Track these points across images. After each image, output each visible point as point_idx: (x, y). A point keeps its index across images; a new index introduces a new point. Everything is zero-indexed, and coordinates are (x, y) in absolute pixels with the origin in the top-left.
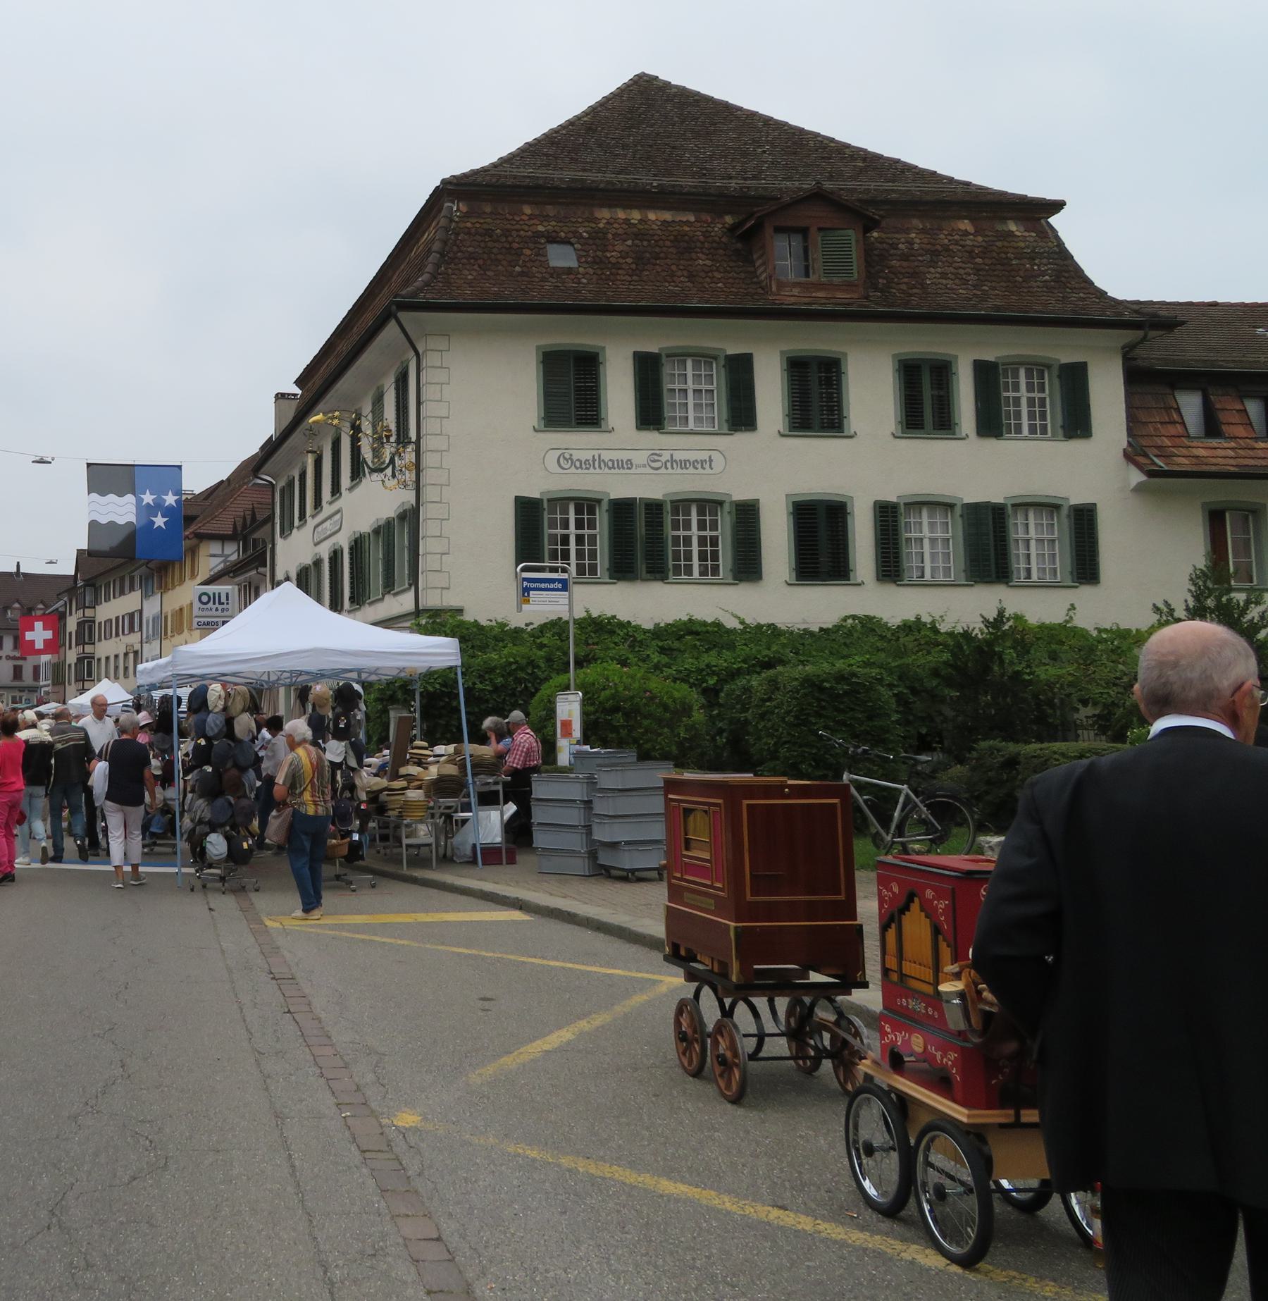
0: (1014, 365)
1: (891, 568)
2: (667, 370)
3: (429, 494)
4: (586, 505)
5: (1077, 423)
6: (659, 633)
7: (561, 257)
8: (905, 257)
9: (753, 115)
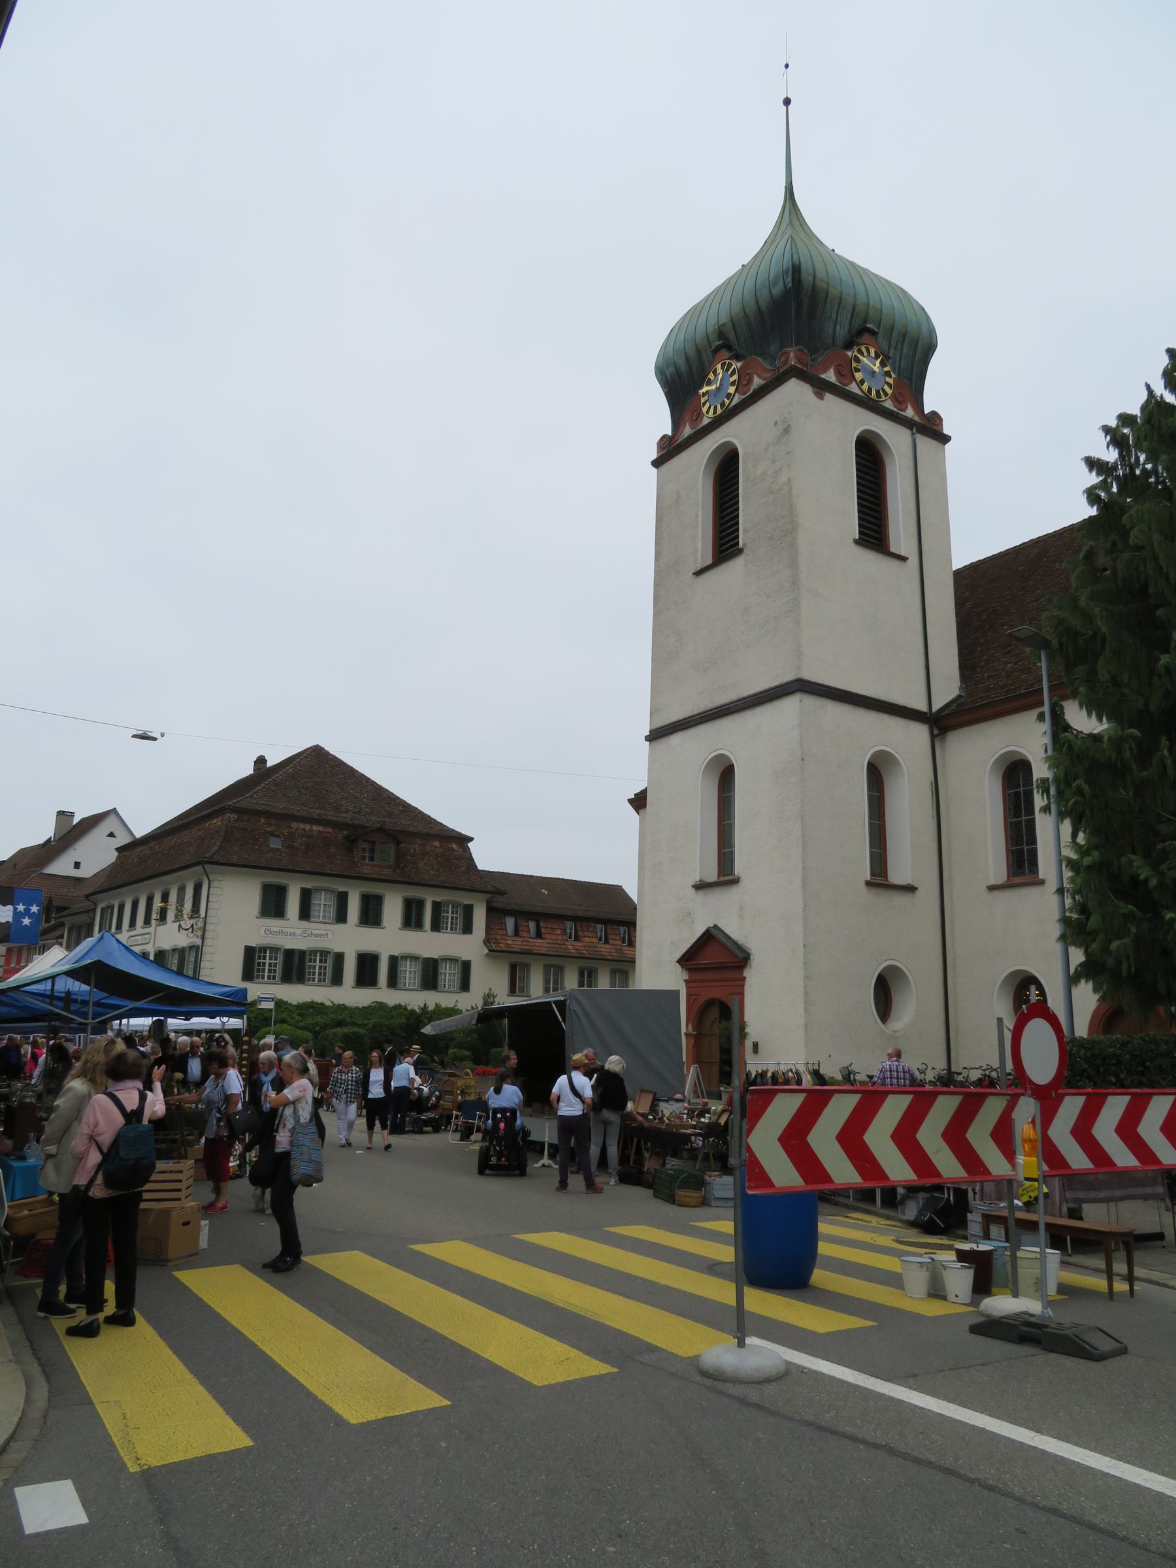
0: (447, 903)
1: (393, 983)
2: (313, 895)
3: (207, 942)
4: (275, 950)
5: (468, 929)
6: (300, 1007)
7: (275, 843)
8: (412, 855)
9: (363, 775)
